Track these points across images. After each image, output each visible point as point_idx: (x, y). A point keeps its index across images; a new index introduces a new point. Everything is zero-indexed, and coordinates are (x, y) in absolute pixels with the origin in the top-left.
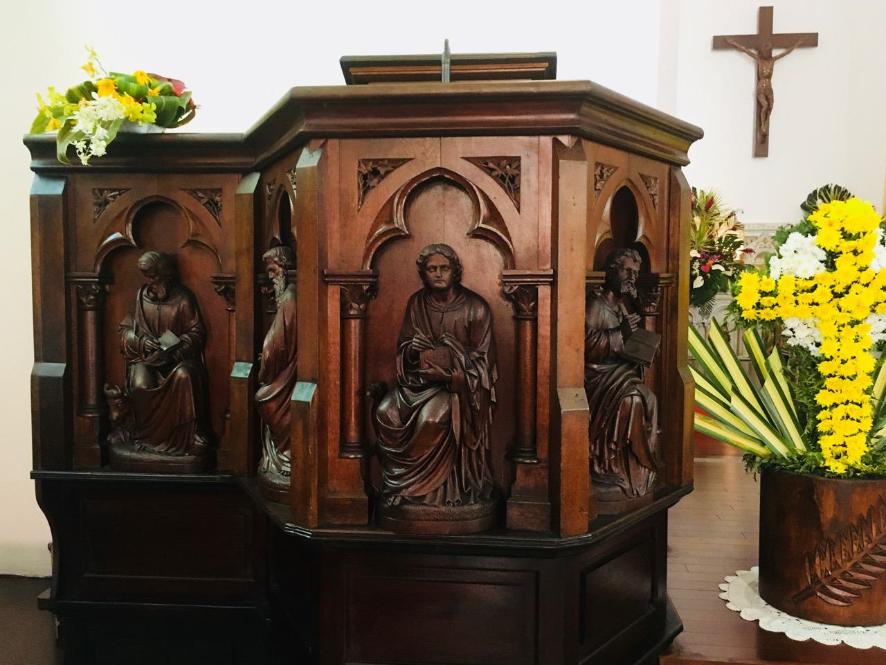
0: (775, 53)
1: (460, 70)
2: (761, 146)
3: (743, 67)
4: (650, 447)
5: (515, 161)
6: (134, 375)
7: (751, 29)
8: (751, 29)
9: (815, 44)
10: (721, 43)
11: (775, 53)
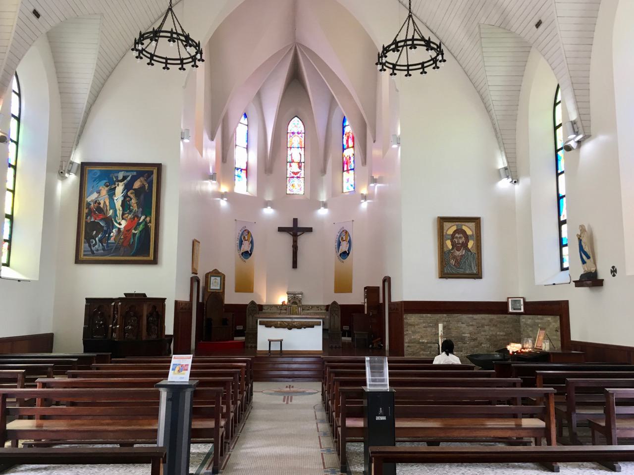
0: (299, 234)
1: (85, 253)
2: (295, 265)
3: (287, 239)
4: (313, 367)
5: (445, 274)
6: (22, 471)
7: (290, 225)
8: (290, 225)
9: (312, 231)
10: (281, 229)
11: (299, 234)
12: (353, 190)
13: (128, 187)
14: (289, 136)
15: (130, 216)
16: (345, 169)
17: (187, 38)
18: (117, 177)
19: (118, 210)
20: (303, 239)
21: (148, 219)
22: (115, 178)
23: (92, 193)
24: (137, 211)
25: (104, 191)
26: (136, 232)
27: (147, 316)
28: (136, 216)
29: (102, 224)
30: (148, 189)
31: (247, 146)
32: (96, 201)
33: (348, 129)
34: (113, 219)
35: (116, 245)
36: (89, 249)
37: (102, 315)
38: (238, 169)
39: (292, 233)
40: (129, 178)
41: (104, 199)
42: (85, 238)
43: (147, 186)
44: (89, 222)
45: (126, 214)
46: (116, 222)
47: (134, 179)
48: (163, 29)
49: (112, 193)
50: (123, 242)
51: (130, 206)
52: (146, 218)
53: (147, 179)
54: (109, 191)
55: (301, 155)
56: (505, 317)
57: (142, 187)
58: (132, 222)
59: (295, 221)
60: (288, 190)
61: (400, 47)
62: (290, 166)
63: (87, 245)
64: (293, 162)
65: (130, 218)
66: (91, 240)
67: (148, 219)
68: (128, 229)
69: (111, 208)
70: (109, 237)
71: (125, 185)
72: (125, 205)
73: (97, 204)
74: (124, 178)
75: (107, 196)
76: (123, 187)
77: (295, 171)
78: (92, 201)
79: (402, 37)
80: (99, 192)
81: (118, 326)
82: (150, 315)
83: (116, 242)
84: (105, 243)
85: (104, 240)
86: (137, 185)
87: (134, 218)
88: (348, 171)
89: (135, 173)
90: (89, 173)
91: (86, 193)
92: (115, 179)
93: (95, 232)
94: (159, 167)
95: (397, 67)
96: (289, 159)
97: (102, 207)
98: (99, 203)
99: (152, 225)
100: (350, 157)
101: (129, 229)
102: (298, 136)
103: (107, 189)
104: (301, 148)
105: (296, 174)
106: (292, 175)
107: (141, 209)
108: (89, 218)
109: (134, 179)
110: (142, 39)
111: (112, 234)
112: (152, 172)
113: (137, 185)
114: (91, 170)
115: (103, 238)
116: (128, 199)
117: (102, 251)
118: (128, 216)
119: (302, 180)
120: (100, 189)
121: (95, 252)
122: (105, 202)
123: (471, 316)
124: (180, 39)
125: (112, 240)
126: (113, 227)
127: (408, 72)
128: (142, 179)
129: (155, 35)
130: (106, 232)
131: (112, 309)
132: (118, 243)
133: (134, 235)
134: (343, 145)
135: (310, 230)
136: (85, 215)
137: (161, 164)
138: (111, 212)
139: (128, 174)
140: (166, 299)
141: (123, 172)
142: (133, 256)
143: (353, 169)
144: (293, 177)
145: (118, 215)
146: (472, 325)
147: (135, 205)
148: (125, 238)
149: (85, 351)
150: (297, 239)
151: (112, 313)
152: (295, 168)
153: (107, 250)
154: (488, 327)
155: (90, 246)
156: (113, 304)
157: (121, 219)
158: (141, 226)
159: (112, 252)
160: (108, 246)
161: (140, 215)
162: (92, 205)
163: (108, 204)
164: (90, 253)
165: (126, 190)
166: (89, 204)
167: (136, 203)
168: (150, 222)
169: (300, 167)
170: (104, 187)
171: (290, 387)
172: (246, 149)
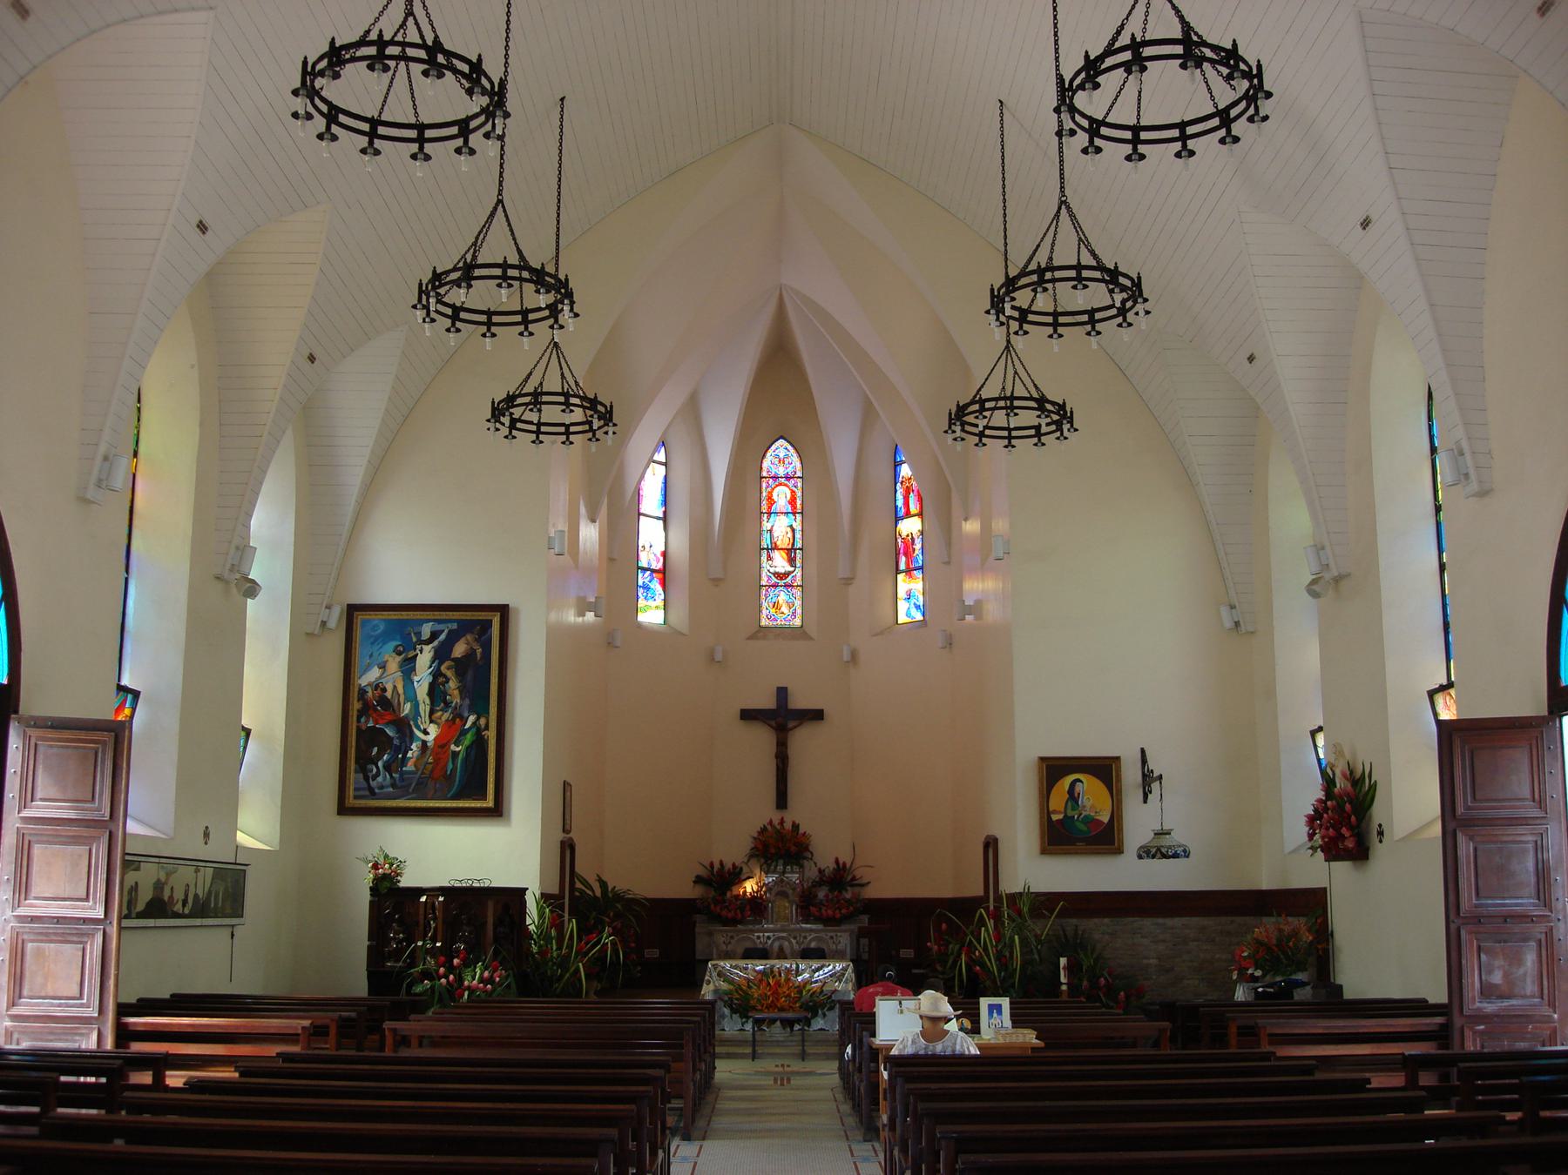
0: (791, 724)
3: (761, 739)
10: (747, 715)
11: (791, 724)
12: (922, 618)
13: (441, 655)
14: (764, 485)
15: (446, 716)
16: (902, 566)
17: (436, 47)
18: (419, 634)
19: (421, 702)
20: (803, 740)
21: (482, 721)
22: (417, 637)
23: (368, 668)
24: (461, 705)
25: (394, 664)
26: (458, 749)
27: (494, 925)
28: (459, 716)
29: (390, 732)
30: (481, 659)
31: (665, 513)
32: (377, 686)
33: (905, 471)
34: (412, 723)
35: (418, 776)
36: (364, 784)
37: (401, 922)
38: (644, 570)
39: (773, 723)
40: (443, 637)
41: (393, 680)
42: (357, 762)
43: (479, 651)
44: (364, 728)
45: (438, 711)
46: (419, 728)
47: (453, 638)
48: (480, 261)
49: (408, 666)
50: (432, 771)
51: (445, 694)
52: (478, 719)
53: (480, 637)
54: (401, 665)
55: (793, 531)
56: (1232, 922)
57: (470, 655)
58: (450, 727)
59: (782, 693)
60: (764, 616)
61: (1032, 272)
62: (769, 558)
63: (361, 775)
64: (775, 548)
65: (447, 720)
66: (369, 766)
67: (482, 721)
68: (442, 743)
69: (407, 700)
70: (404, 760)
71: (436, 652)
72: (435, 692)
73: (379, 689)
74: (434, 635)
75: (400, 674)
76: (432, 653)
77: (782, 570)
78: (369, 684)
79: (990, 391)
80: (383, 667)
81: (438, 944)
82: (499, 923)
83: (417, 770)
84: (396, 772)
85: (394, 767)
86: (459, 650)
87: (453, 720)
88: (909, 571)
89: (455, 626)
90: (362, 626)
91: (357, 670)
92: (414, 639)
93: (376, 749)
94: (503, 610)
95: (1031, 317)
96: (766, 542)
97: (389, 697)
98: (384, 690)
99: (491, 735)
100: (913, 539)
101: (445, 741)
102: (786, 485)
103: (399, 659)
104: (794, 513)
105: (781, 579)
106: (774, 580)
107: (467, 702)
108: (363, 720)
109: (453, 638)
110: (437, 283)
111: (410, 754)
112: (489, 623)
113: (459, 650)
114: (369, 620)
115: (394, 762)
116: (441, 680)
117: (391, 789)
118: (442, 715)
119: (798, 592)
120: (385, 659)
121: (377, 791)
122: (395, 687)
123: (1161, 921)
124: (409, 59)
125: (410, 767)
126: (412, 737)
127: (1010, 442)
128: (469, 637)
129: (468, 272)
130: (397, 750)
131: (422, 911)
132: (423, 773)
133: (455, 754)
134: (896, 507)
135: (817, 715)
136: (355, 713)
137: (508, 605)
138: (407, 709)
139: (439, 627)
140: (527, 889)
141: (431, 623)
142: (456, 797)
143: (921, 568)
144: (775, 586)
145: (422, 714)
146: (1164, 941)
147: (456, 692)
148: (437, 761)
149: (369, 995)
150: (787, 738)
151: (422, 917)
152: (780, 563)
153: (402, 787)
154: (1195, 943)
155: (366, 778)
156: (423, 899)
157: (428, 723)
158: (468, 739)
159: (411, 790)
160: (402, 779)
161: (466, 714)
162: (370, 694)
163: (401, 690)
164: (367, 793)
165: (437, 661)
166: (362, 692)
167: (458, 688)
168: (487, 728)
169: (792, 561)
170: (394, 655)
171: (783, 1066)
172: (661, 523)
